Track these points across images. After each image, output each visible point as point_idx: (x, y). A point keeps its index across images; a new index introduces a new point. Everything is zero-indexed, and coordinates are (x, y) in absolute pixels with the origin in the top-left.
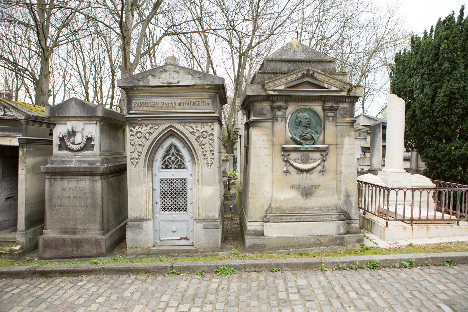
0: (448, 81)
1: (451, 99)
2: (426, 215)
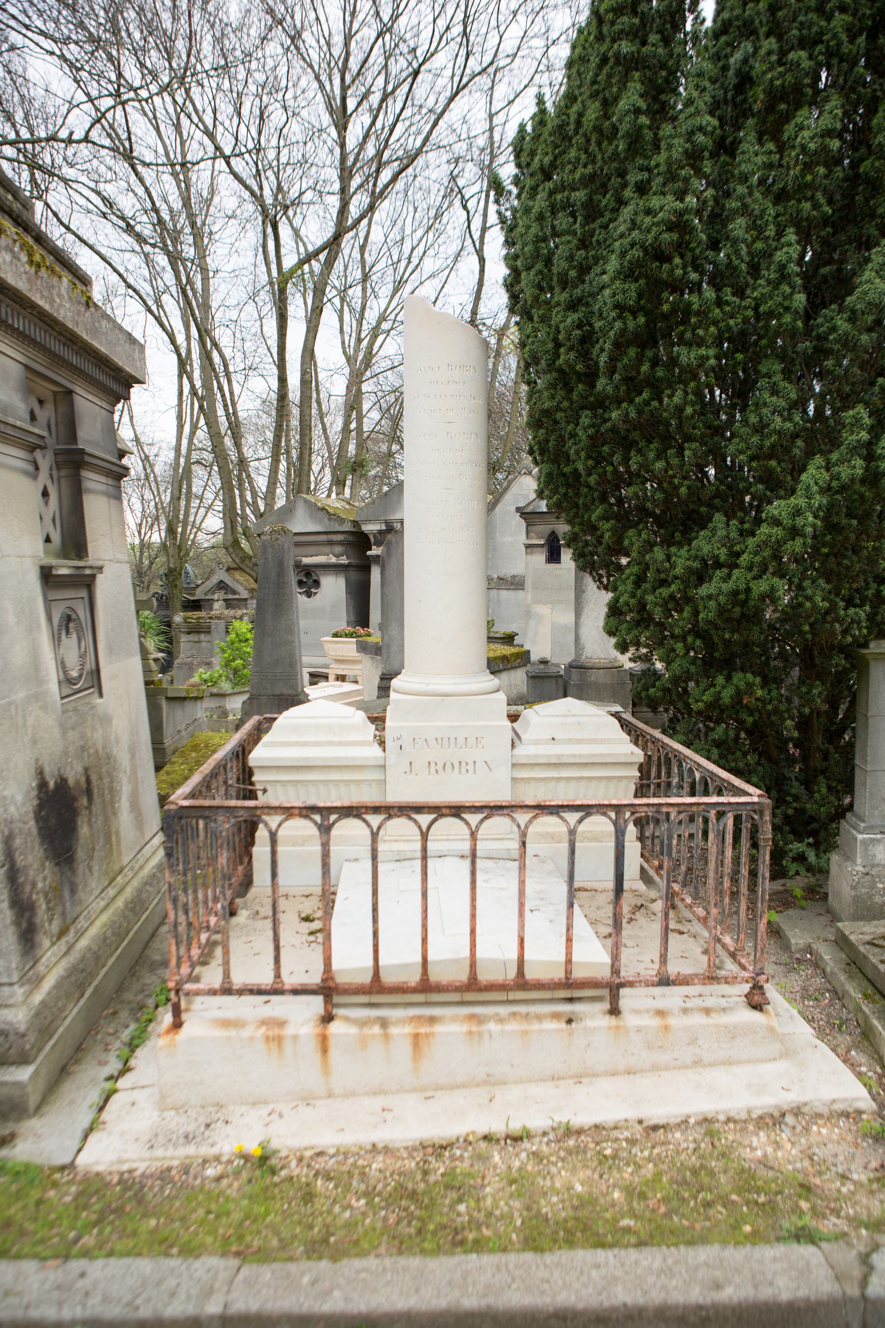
0: (642, 189)
1: (655, 288)
2: (370, 963)
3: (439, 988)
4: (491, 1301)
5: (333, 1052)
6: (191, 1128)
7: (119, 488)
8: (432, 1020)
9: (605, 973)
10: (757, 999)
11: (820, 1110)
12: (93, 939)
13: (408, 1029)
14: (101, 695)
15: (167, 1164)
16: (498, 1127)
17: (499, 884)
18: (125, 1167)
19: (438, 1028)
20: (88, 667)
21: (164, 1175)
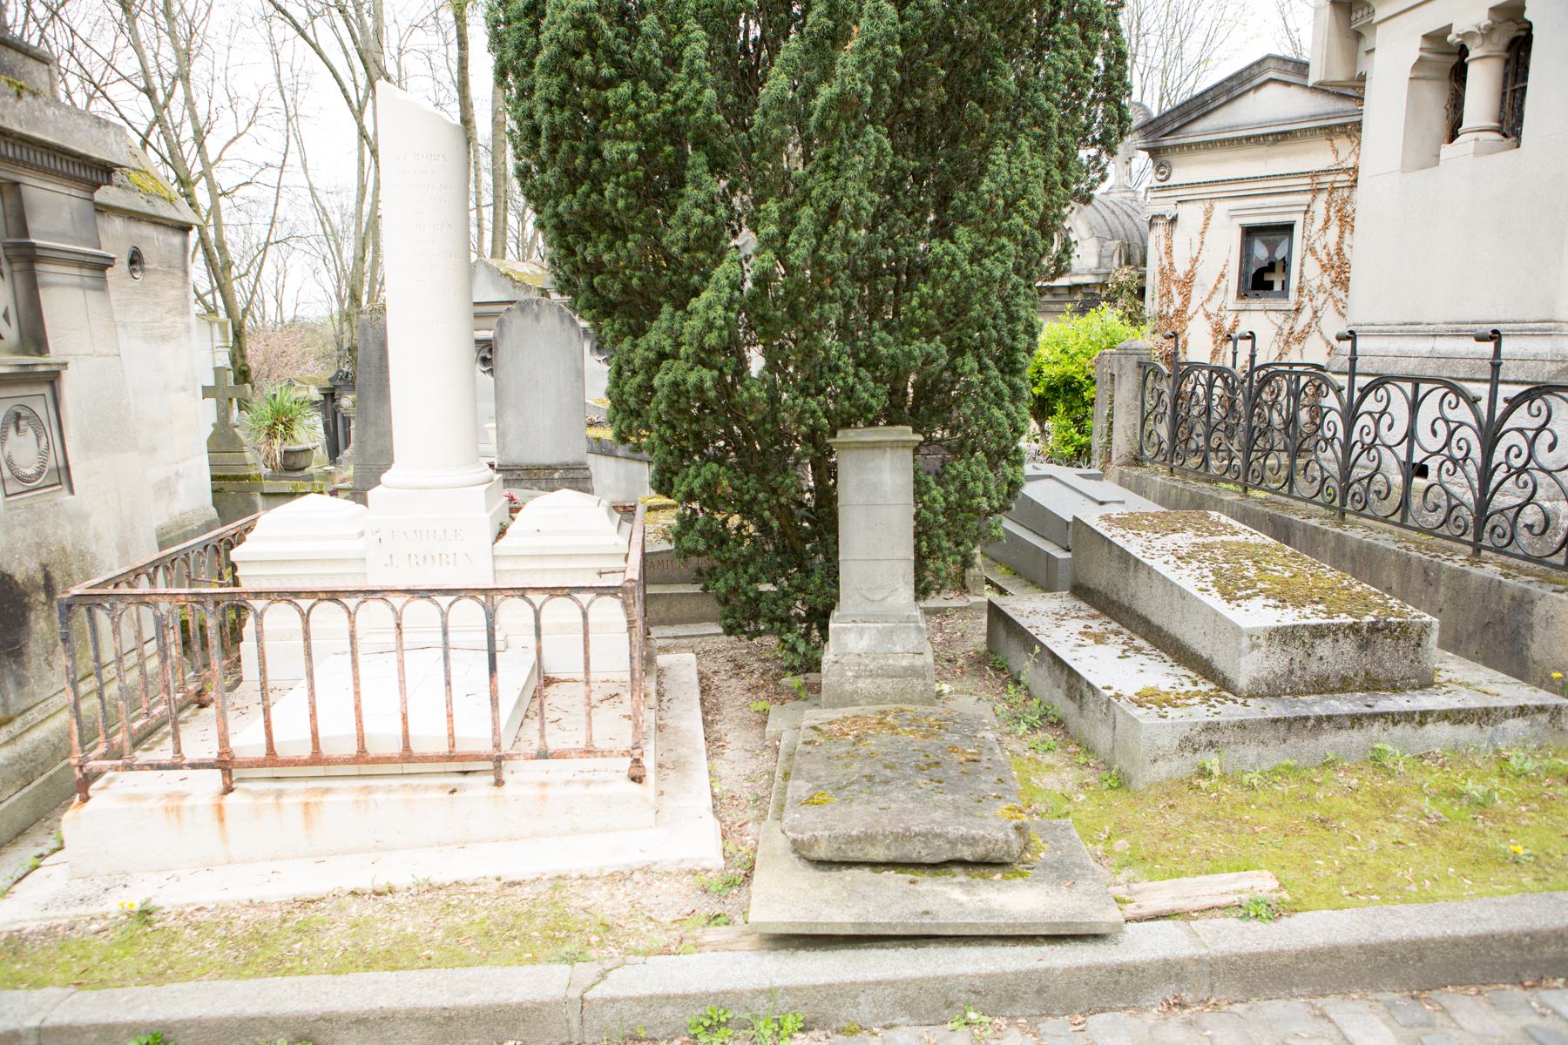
3: (328, 762)
4: (270, 1008)
5: (229, 820)
6: (88, 893)
7: (104, 278)
8: (327, 791)
9: (486, 747)
10: (637, 772)
11: (668, 869)
12: (53, 732)
13: (301, 799)
14: (72, 491)
15: (56, 922)
16: (365, 884)
17: (424, 666)
18: (17, 927)
19: (328, 798)
20: (51, 463)
21: (50, 932)
